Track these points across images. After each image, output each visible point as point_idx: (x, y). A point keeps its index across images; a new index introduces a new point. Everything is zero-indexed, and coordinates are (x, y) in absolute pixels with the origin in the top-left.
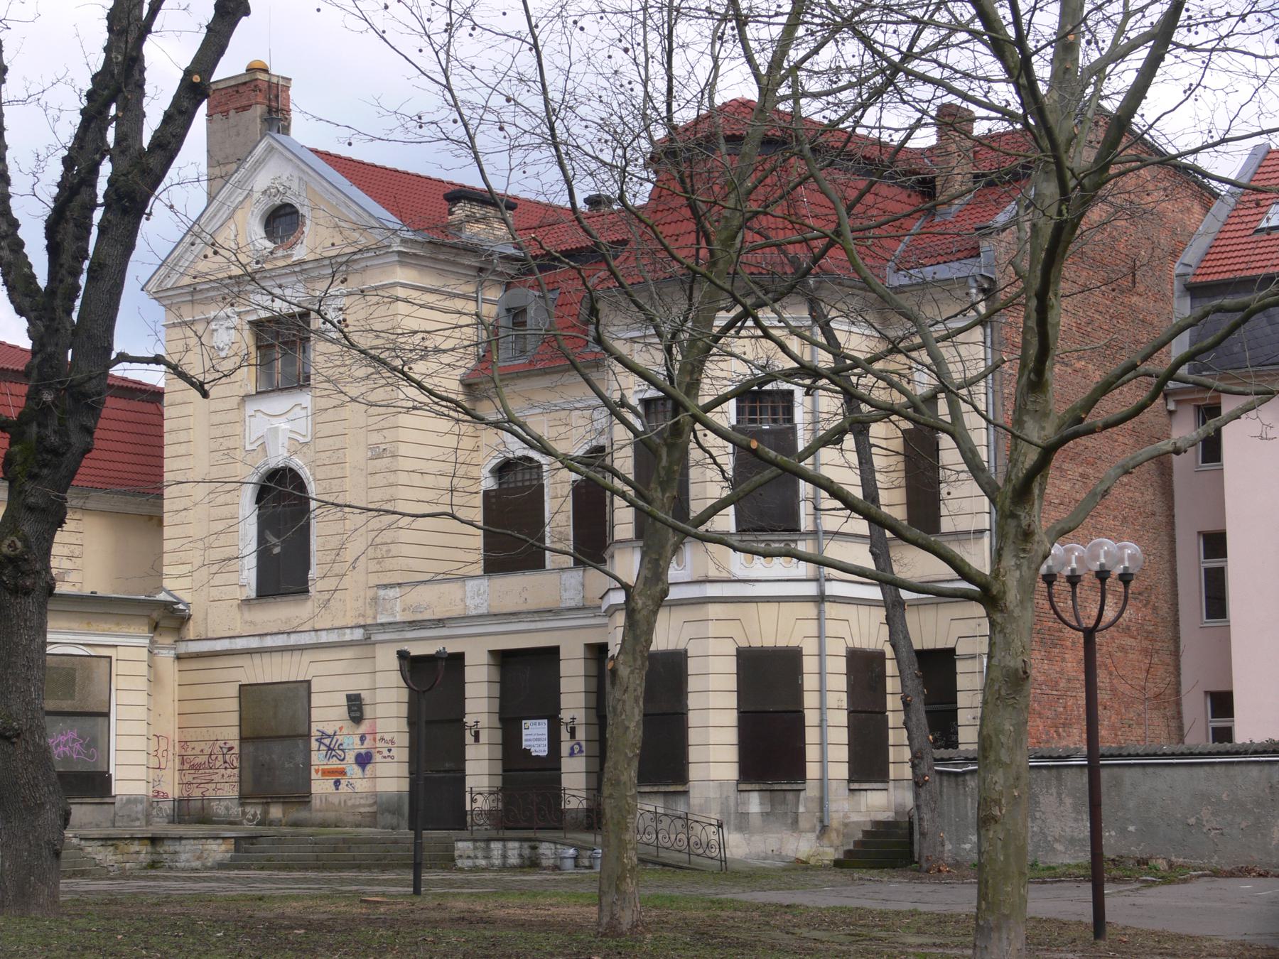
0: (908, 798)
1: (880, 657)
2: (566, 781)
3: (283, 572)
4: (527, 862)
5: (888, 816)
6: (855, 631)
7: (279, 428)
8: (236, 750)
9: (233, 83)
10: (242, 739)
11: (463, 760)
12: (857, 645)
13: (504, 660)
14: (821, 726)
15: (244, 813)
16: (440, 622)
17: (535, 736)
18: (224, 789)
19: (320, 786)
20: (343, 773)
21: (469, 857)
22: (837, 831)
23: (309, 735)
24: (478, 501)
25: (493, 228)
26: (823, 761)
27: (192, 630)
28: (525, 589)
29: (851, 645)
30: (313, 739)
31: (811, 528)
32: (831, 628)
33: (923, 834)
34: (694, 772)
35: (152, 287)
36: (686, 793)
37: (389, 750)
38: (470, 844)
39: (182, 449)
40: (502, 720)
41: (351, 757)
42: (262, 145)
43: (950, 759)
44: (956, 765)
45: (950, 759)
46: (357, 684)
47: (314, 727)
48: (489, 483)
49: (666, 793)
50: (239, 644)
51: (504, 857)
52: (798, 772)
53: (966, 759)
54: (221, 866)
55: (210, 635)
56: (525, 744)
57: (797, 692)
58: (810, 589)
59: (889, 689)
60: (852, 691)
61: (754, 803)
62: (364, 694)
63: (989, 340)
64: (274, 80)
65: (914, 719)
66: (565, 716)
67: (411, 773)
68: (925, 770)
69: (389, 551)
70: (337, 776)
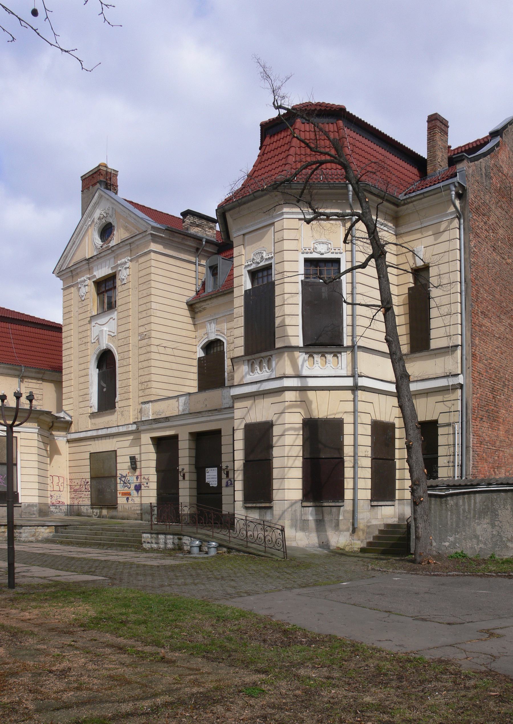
0: (408, 511)
1: (391, 427)
2: (181, 492)
3: (107, 401)
4: (177, 547)
5: (394, 521)
6: (377, 409)
7: (105, 331)
8: (89, 483)
9: (91, 173)
10: (91, 478)
11: (178, 489)
12: (378, 418)
14: (354, 467)
15: (93, 512)
17: (211, 476)
18: (85, 500)
19: (121, 500)
20: (129, 494)
21: (148, 543)
22: (363, 531)
23: (116, 476)
24: (195, 363)
25: (206, 231)
26: (355, 489)
27: (73, 428)
28: (206, 399)
29: (374, 418)
30: (118, 478)
31: (350, 344)
32: (361, 407)
33: (417, 538)
34: (276, 495)
35: (57, 271)
36: (271, 508)
37: (147, 484)
38: (149, 535)
39: (68, 346)
40: (196, 468)
41: (133, 487)
42: (97, 194)
43: (437, 486)
44: (441, 490)
45: (437, 486)
46: (134, 451)
47: (119, 472)
48: (201, 354)
49: (260, 508)
50: (89, 434)
51: (166, 543)
52: (339, 495)
53: (448, 486)
54: (47, 541)
55: (80, 431)
56: (207, 480)
57: (340, 447)
58: (349, 382)
59: (397, 435)
60: (374, 446)
62: (137, 457)
63: (462, 226)
64: (109, 171)
65: (414, 458)
66: (224, 466)
67: (158, 495)
68: (421, 493)
69: (147, 385)
70: (127, 495)
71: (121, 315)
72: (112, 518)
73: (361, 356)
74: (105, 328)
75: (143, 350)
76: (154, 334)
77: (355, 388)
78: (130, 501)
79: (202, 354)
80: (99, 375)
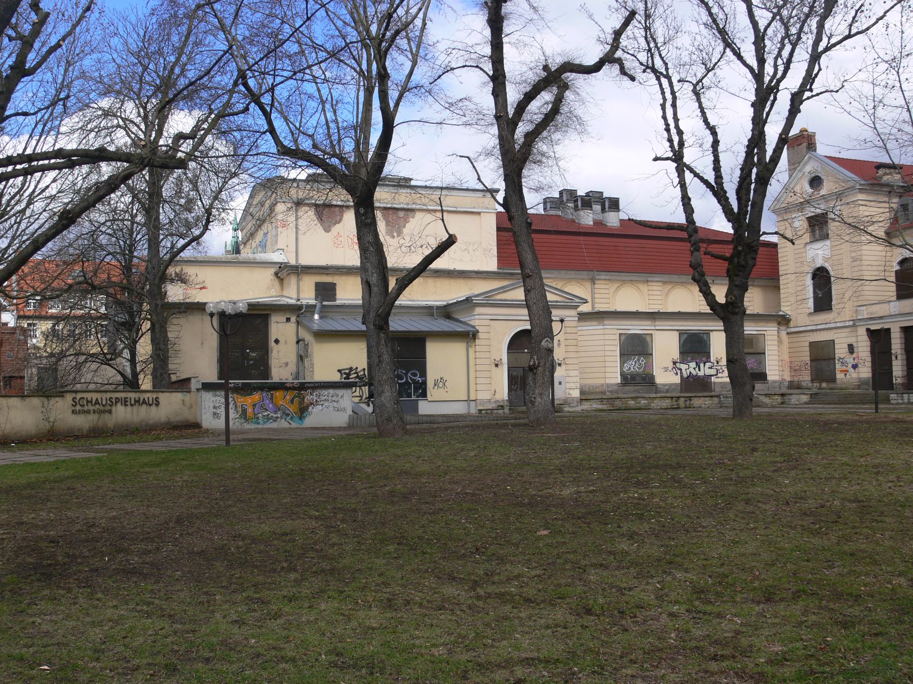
7: (819, 253)
10: (811, 360)
11: (892, 366)
16: (881, 318)
18: (805, 377)
19: (839, 376)
24: (893, 274)
27: (792, 324)
41: (850, 366)
46: (851, 340)
54: (806, 403)
71: (834, 244)
72: (831, 389)
74: (820, 252)
75: (856, 269)
76: (864, 258)
78: (848, 376)
79: (898, 268)
80: (814, 285)
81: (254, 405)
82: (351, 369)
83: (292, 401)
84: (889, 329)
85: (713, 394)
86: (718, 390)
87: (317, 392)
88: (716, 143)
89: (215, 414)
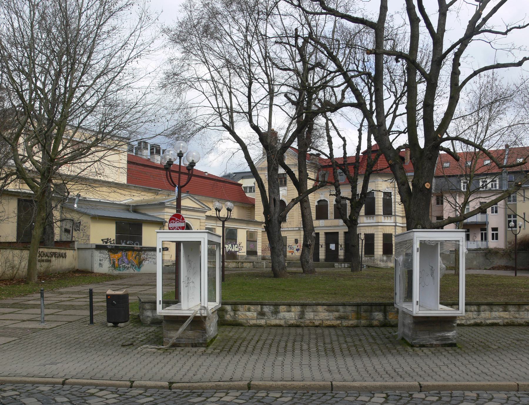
13: (326, 234)
19: (288, 254)
23: (286, 245)
32: (397, 230)
34: (375, 253)
41: (295, 249)
46: (297, 237)
58: (394, 224)
61: (385, 258)
70: (292, 253)
73: (397, 217)
77: (396, 226)
81: (119, 260)
82: (108, 239)
83: (136, 257)
84: (319, 233)
85: (237, 261)
86: (240, 259)
87: (147, 253)
88: (344, 145)
89: (100, 264)
